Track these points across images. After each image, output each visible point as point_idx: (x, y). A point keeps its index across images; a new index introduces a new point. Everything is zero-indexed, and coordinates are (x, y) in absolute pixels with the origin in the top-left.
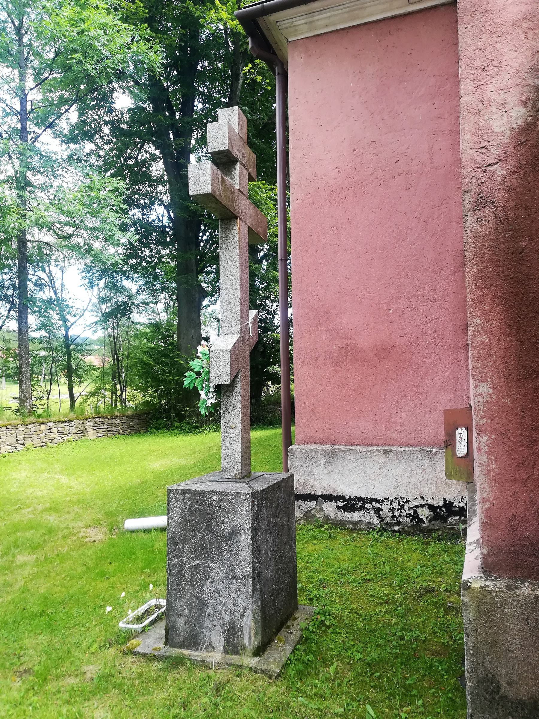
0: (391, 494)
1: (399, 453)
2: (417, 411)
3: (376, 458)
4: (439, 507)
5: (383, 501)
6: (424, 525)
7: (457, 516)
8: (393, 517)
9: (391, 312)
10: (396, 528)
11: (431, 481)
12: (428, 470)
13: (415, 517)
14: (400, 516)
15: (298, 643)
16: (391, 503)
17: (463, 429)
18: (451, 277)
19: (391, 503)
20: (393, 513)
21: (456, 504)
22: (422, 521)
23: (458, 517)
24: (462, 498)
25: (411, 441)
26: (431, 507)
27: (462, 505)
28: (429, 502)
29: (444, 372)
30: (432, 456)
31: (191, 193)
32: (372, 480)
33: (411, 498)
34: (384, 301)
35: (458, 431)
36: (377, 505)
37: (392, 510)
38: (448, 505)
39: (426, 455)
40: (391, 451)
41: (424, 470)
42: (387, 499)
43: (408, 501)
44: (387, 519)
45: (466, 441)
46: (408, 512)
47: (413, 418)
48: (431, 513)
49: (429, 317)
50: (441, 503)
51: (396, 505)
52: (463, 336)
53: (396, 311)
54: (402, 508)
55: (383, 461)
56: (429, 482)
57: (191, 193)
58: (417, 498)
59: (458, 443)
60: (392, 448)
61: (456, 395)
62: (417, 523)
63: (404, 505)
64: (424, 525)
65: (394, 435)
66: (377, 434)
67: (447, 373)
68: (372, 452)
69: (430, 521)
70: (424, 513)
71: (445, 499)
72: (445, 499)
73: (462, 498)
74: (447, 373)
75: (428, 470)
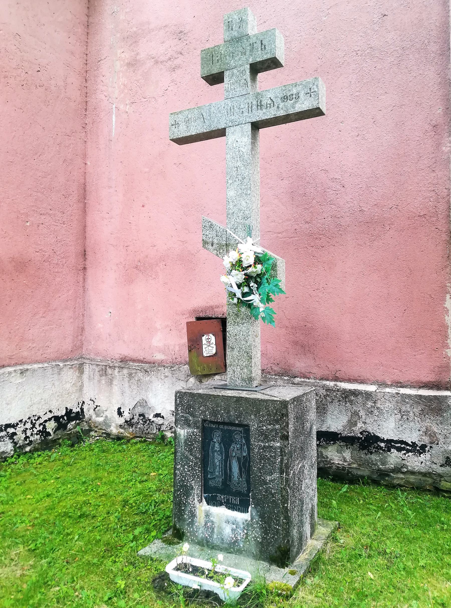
0: (25, 415)
1: (34, 370)
2: (47, 328)
3: (13, 380)
4: (62, 417)
5: (17, 424)
6: (50, 437)
7: (73, 421)
8: (27, 437)
9: (28, 224)
10: (28, 449)
11: (58, 394)
12: (57, 383)
13: (44, 433)
14: (32, 435)
15: (95, 472)
16: (24, 425)
17: (211, 335)
18: (75, 205)
19: (24, 425)
20: (26, 434)
21: (75, 410)
22: (49, 434)
23: (74, 422)
24: (79, 404)
25: (38, 358)
26: (57, 419)
27: (78, 409)
28: (55, 414)
29: (68, 291)
30: (61, 369)
31: (205, 354)
32: (8, 404)
33: (41, 414)
34: (22, 212)
35: (204, 338)
36: (11, 430)
37: (25, 431)
38: (69, 412)
39: (56, 369)
40: (27, 370)
41: (53, 384)
42: (21, 421)
43: (39, 418)
44: (20, 442)
45: (214, 343)
46: (38, 429)
47: (43, 334)
48: (56, 424)
49: (58, 238)
50: (64, 413)
51: (29, 425)
52: (82, 260)
53: (32, 225)
54: (34, 425)
55: (20, 381)
56: (57, 395)
57: (205, 354)
58: (46, 413)
59: (204, 347)
60: (29, 367)
61: (75, 312)
62: (45, 437)
63: (35, 423)
64: (50, 437)
65: (25, 354)
66: (9, 354)
67: (70, 293)
68: (10, 373)
69: (54, 433)
70: (51, 426)
71: (67, 408)
72: (67, 408)
73: (79, 404)
74: (70, 293)
75: (57, 383)
